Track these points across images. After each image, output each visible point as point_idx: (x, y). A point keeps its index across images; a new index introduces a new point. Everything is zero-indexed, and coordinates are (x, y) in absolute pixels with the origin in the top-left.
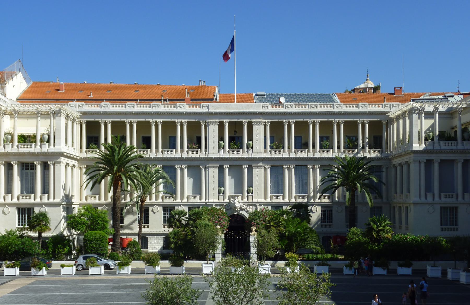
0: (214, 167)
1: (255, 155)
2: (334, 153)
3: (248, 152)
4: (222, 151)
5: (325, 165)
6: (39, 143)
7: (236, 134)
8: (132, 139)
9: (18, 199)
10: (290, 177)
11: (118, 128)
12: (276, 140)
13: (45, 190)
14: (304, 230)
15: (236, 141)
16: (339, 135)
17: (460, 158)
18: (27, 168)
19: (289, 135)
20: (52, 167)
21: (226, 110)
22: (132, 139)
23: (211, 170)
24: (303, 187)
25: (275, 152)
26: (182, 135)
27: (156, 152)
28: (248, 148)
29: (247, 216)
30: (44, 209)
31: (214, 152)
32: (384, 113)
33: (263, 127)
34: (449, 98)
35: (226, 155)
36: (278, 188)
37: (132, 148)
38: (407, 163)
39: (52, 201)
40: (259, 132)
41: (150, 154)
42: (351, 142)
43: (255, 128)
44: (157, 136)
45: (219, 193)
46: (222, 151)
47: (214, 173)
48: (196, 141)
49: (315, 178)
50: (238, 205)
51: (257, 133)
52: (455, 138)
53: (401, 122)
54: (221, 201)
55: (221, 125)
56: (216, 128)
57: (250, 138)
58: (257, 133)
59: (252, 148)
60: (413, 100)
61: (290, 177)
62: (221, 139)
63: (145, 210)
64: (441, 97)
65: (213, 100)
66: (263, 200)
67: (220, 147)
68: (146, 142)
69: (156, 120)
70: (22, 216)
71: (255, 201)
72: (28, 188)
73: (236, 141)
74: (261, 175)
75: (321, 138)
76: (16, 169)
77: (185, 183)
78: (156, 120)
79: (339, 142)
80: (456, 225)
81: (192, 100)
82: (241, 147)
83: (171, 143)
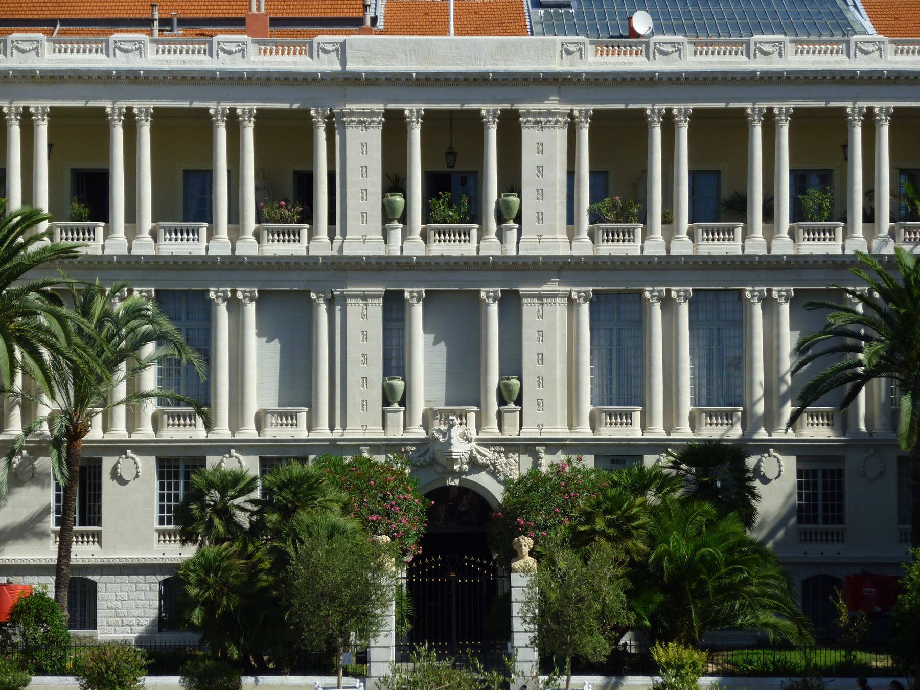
1: (531, 247)
3: (500, 235)
4: (396, 235)
5: (816, 289)
7: (455, 161)
10: (671, 338)
12: (616, 183)
15: (453, 192)
19: (670, 167)
23: (354, 309)
24: (722, 380)
25: (613, 235)
26: (236, 167)
28: (501, 219)
29: (497, 491)
31: (364, 238)
33: (560, 135)
35: (415, 248)
36: (622, 382)
40: (548, 154)
41: (109, 241)
43: (530, 137)
44: (133, 169)
45: (386, 402)
47: (364, 320)
48: (291, 193)
49: (775, 339)
50: (460, 449)
51: (538, 159)
54: (396, 432)
55: (394, 129)
56: (374, 137)
57: (511, 181)
58: (538, 159)
59: (518, 220)
61: (671, 338)
62: (395, 182)
65: (359, 22)
66: (561, 431)
67: (387, 215)
68: (88, 194)
71: (530, 432)
73: (453, 192)
74: (556, 330)
75: (799, 180)
77: (248, 361)
79: (870, 194)
81: (275, 22)
82: (475, 215)
83: (188, 200)
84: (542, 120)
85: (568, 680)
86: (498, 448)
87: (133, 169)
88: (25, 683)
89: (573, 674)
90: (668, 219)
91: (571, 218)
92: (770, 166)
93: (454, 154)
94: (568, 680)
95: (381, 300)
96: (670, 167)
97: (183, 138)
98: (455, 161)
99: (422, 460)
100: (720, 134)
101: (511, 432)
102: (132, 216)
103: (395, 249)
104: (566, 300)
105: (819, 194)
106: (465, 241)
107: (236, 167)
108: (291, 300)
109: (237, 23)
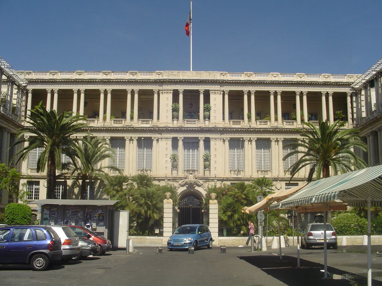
0: (167, 138)
2: (297, 125)
7: (192, 102)
8: (78, 107)
14: (235, 211)
15: (191, 112)
16: (302, 110)
19: (250, 107)
25: (234, 123)
27: (105, 120)
32: (347, 85)
37: (78, 117)
40: (218, 103)
41: (97, 123)
42: (315, 114)
43: (212, 97)
44: (105, 105)
48: (146, 111)
55: (176, 94)
57: (207, 109)
62: (175, 110)
67: (173, 118)
68: (92, 112)
69: (277, 137)
70: (29, 186)
71: (212, 175)
73: (191, 112)
78: (277, 137)
80: (323, 245)
83: (119, 112)
85: (267, 238)
86: (203, 180)
89: (268, 236)
90: (249, 117)
91: (224, 119)
93: (192, 104)
94: (267, 238)
95: (171, 140)
96: (250, 107)
97: (119, 97)
98: (192, 102)
99: (182, 183)
104: (222, 140)
105: (288, 114)
106: (195, 124)
107: (132, 106)
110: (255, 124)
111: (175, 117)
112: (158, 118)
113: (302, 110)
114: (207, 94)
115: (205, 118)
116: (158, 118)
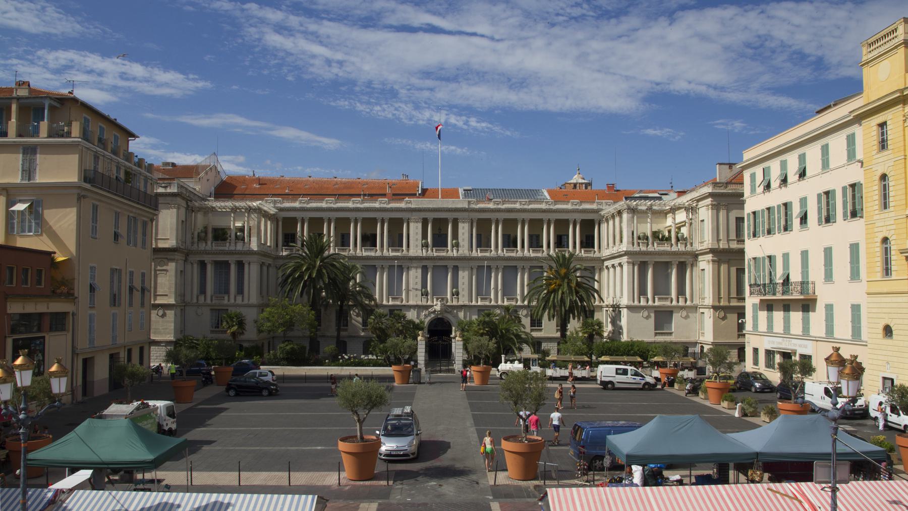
2: (544, 253)
5: (534, 267)
6: (210, 230)
7: (439, 229)
9: (212, 300)
10: (497, 280)
11: (316, 224)
13: (681, 291)
15: (440, 241)
16: (548, 235)
17: (675, 260)
18: (222, 267)
19: (496, 235)
20: (246, 266)
21: (431, 206)
22: (329, 233)
24: (508, 290)
26: (382, 233)
30: (238, 310)
32: (597, 211)
34: (663, 197)
38: (620, 265)
39: (246, 302)
42: (561, 241)
43: (461, 225)
46: (424, 300)
48: (396, 241)
49: (522, 282)
52: (669, 239)
53: (611, 223)
55: (425, 222)
56: (420, 225)
57: (455, 236)
60: (626, 198)
61: (497, 280)
62: (424, 236)
63: (85, 181)
64: (657, 195)
66: (467, 303)
68: (343, 241)
72: (661, 290)
75: (530, 236)
76: (209, 268)
81: (394, 195)
84: (464, 269)
87: (355, 232)
88: (357, 508)
92: (522, 233)
96: (496, 235)
100: (510, 225)
101: (455, 303)
102: (382, 246)
103: (425, 254)
108: (482, 270)
109: (384, 195)
110: (528, 253)
111: (425, 245)
112: (408, 246)
113: (548, 235)
114: (455, 223)
115: (453, 246)
116: (408, 246)
